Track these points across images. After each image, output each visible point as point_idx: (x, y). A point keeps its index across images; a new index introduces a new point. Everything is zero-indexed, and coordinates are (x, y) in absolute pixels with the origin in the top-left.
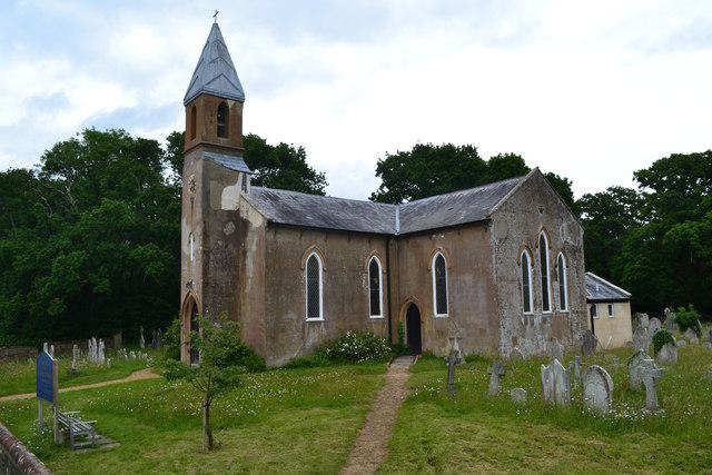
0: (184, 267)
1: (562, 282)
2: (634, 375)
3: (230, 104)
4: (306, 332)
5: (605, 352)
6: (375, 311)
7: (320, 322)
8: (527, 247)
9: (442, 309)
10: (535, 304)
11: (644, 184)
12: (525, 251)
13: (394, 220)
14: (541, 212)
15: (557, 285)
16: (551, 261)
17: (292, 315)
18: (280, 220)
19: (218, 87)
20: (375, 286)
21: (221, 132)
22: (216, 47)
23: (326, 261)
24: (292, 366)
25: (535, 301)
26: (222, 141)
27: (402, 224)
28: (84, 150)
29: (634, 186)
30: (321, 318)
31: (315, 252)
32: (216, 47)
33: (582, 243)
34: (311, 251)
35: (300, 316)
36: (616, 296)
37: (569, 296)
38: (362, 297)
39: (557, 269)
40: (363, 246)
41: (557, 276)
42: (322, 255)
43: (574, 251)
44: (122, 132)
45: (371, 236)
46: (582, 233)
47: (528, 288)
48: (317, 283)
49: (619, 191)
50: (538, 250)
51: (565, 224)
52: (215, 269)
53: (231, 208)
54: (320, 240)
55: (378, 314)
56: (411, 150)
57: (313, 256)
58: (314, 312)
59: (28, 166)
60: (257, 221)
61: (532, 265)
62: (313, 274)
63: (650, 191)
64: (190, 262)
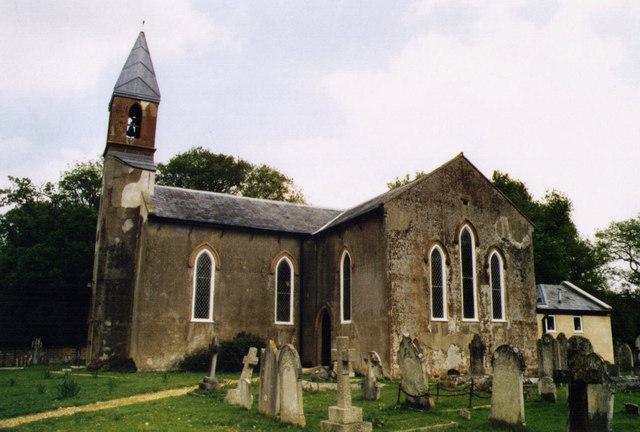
1: (496, 285)
2: (259, 408)
3: (144, 105)
4: (191, 332)
6: (284, 316)
7: (208, 323)
8: (440, 242)
9: (347, 317)
10: (451, 307)
12: (495, 251)
14: (465, 203)
15: (488, 290)
16: (478, 261)
19: (136, 90)
22: (141, 44)
23: (221, 259)
24: (195, 364)
31: (206, 250)
32: (141, 44)
34: (283, 255)
35: (185, 317)
36: (596, 308)
39: (489, 271)
40: (270, 244)
42: (216, 251)
45: (280, 235)
47: (441, 290)
50: (459, 248)
53: (134, 205)
54: (214, 237)
55: (206, 316)
57: (205, 255)
58: (202, 312)
61: (448, 263)
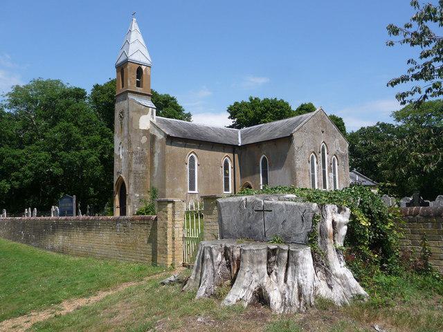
0: (116, 163)
1: (334, 173)
5: (165, 147)
11: (398, 120)
13: (239, 138)
15: (332, 175)
16: (328, 161)
17: (180, 189)
18: (173, 135)
20: (226, 175)
21: (139, 84)
25: (318, 183)
26: (139, 90)
27: (242, 140)
28: (400, 133)
29: (391, 121)
30: (196, 191)
33: (347, 151)
37: (339, 183)
38: (219, 180)
41: (332, 170)
43: (342, 156)
44: (58, 82)
46: (348, 146)
48: (194, 171)
49: (383, 125)
50: (321, 155)
51: (337, 140)
52: (136, 163)
56: (262, 99)
58: (192, 188)
59: (276, 172)
60: (160, 136)
61: (317, 163)
62: (192, 166)
63: (400, 124)
64: (120, 160)
